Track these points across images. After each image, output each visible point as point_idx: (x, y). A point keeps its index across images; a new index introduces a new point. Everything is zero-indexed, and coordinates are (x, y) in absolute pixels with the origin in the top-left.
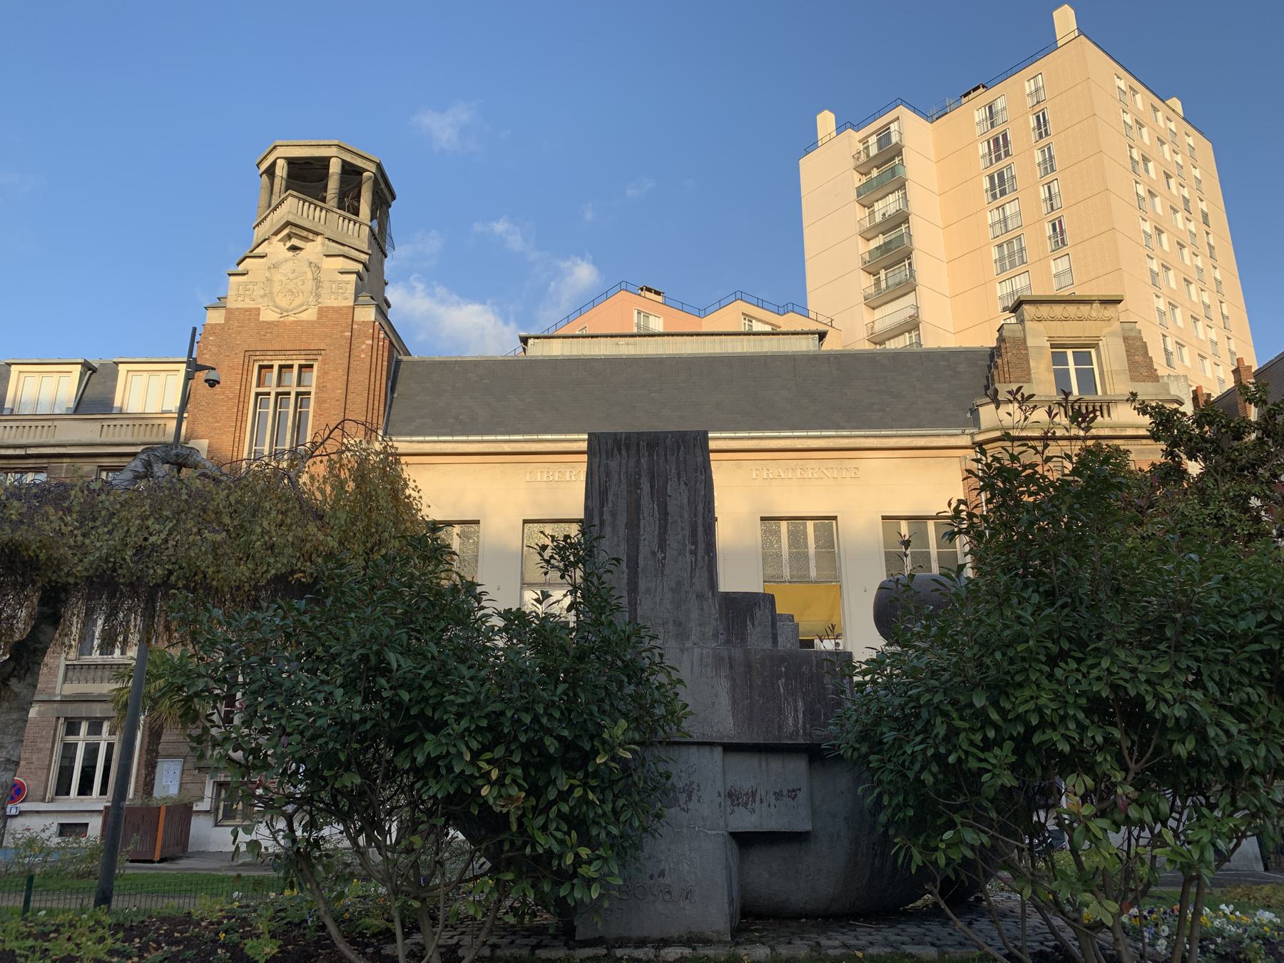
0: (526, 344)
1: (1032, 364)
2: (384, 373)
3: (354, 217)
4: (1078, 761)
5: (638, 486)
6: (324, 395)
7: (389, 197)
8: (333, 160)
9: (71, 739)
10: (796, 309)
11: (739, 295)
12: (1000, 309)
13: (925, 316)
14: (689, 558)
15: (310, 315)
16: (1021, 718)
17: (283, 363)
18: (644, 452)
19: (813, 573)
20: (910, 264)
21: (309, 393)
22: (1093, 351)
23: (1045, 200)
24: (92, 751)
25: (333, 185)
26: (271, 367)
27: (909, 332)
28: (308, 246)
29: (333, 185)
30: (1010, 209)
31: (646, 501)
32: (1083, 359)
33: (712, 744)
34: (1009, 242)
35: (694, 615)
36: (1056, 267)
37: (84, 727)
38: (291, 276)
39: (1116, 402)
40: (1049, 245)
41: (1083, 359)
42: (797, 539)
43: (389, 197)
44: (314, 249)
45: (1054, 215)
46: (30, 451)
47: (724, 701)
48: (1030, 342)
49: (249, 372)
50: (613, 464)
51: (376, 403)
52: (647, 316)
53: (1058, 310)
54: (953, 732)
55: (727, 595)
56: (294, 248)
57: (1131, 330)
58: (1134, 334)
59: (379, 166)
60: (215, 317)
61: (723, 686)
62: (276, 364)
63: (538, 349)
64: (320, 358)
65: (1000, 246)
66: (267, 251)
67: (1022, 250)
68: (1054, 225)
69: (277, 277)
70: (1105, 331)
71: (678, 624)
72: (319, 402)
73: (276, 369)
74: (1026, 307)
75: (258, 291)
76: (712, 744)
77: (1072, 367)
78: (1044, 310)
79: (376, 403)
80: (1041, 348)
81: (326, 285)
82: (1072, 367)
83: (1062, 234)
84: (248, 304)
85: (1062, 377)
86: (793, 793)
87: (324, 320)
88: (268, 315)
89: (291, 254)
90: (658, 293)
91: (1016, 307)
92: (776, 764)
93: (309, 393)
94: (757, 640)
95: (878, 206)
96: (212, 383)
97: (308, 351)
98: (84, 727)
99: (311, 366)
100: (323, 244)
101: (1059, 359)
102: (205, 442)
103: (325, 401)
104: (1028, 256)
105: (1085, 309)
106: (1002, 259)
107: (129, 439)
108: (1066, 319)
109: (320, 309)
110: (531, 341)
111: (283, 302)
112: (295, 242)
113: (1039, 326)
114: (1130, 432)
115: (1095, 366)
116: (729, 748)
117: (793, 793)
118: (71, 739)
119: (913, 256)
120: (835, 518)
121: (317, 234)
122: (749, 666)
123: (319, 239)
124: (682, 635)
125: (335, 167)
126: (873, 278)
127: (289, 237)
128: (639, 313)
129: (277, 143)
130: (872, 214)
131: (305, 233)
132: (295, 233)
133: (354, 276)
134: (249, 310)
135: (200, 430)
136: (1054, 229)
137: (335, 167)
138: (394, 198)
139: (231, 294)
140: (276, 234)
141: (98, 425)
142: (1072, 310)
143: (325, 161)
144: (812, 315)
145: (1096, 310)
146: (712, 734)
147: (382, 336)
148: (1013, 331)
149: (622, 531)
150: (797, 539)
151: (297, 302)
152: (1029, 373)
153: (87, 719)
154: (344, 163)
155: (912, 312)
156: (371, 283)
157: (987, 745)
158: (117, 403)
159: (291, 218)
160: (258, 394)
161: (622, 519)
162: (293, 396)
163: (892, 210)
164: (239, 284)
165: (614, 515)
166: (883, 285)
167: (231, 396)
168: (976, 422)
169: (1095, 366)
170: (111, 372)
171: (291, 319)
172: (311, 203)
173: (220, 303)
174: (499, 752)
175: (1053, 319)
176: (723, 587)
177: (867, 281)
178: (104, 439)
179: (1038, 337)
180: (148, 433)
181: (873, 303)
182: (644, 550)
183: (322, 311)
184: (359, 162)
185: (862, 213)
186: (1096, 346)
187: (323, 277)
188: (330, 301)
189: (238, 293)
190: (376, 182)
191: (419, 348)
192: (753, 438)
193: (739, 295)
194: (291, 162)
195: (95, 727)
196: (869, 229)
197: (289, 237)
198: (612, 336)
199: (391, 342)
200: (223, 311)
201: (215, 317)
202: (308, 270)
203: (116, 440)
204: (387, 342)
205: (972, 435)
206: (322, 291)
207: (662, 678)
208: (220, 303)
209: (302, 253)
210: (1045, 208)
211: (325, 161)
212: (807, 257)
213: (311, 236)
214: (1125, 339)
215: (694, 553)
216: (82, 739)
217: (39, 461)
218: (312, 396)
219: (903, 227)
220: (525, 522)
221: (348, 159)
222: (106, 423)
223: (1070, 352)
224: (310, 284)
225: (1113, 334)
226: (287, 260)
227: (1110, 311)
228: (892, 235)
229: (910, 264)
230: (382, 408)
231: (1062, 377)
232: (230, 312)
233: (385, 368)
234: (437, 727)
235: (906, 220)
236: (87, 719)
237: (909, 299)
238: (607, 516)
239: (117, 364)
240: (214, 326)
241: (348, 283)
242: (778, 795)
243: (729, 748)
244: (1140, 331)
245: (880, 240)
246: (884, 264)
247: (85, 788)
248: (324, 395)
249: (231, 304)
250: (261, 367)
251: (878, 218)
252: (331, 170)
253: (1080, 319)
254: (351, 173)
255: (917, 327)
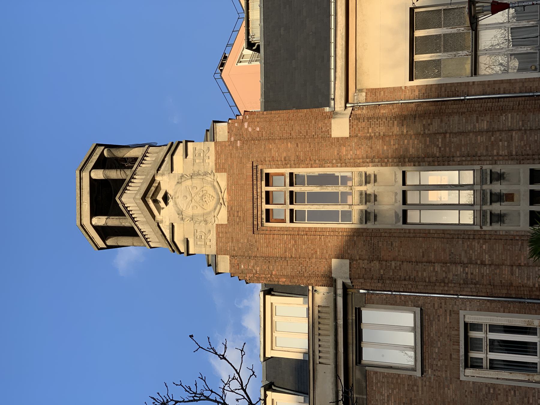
3: (139, 160)
6: (293, 158)
15: (222, 179)
17: (264, 200)
25: (114, 174)
26: (268, 211)
28: (164, 187)
29: (114, 174)
38: (189, 198)
42: (427, 45)
44: (166, 182)
46: (341, 322)
49: (272, 229)
56: (166, 198)
60: (224, 264)
63: (257, 35)
64: (260, 167)
69: (189, 212)
72: (299, 163)
75: (202, 228)
81: (196, 168)
84: (213, 236)
87: (226, 166)
88: (223, 217)
89: (171, 202)
93: (291, 174)
99: (267, 175)
100: (163, 175)
102: (334, 261)
103: (298, 157)
107: (331, 338)
109: (217, 170)
111: (212, 203)
112: (160, 197)
120: (412, 10)
121: (153, 180)
123: (158, 178)
125: (98, 175)
127: (156, 201)
129: (78, 223)
131: (153, 189)
134: (218, 234)
135: (322, 268)
139: (203, 251)
140: (154, 216)
141: (319, 367)
150: (427, 45)
151: (211, 191)
154: (95, 167)
158: (300, 357)
159: (139, 196)
164: (196, 244)
167: (293, 242)
170: (272, 363)
171: (226, 196)
173: (212, 263)
178: (331, 361)
180: (326, 321)
183: (219, 168)
187: (189, 172)
189: (204, 245)
194: (94, 213)
197: (156, 201)
200: (220, 257)
201: (224, 264)
203: (332, 350)
206: (202, 171)
208: (212, 263)
209: (171, 193)
211: (93, 182)
213: (155, 185)
217: (350, 341)
221: (93, 164)
222: (318, 360)
224: (196, 181)
232: (221, 251)
239: (266, 359)
240: (232, 265)
241: (195, 149)
248: (293, 158)
249: (212, 251)
250: (268, 220)
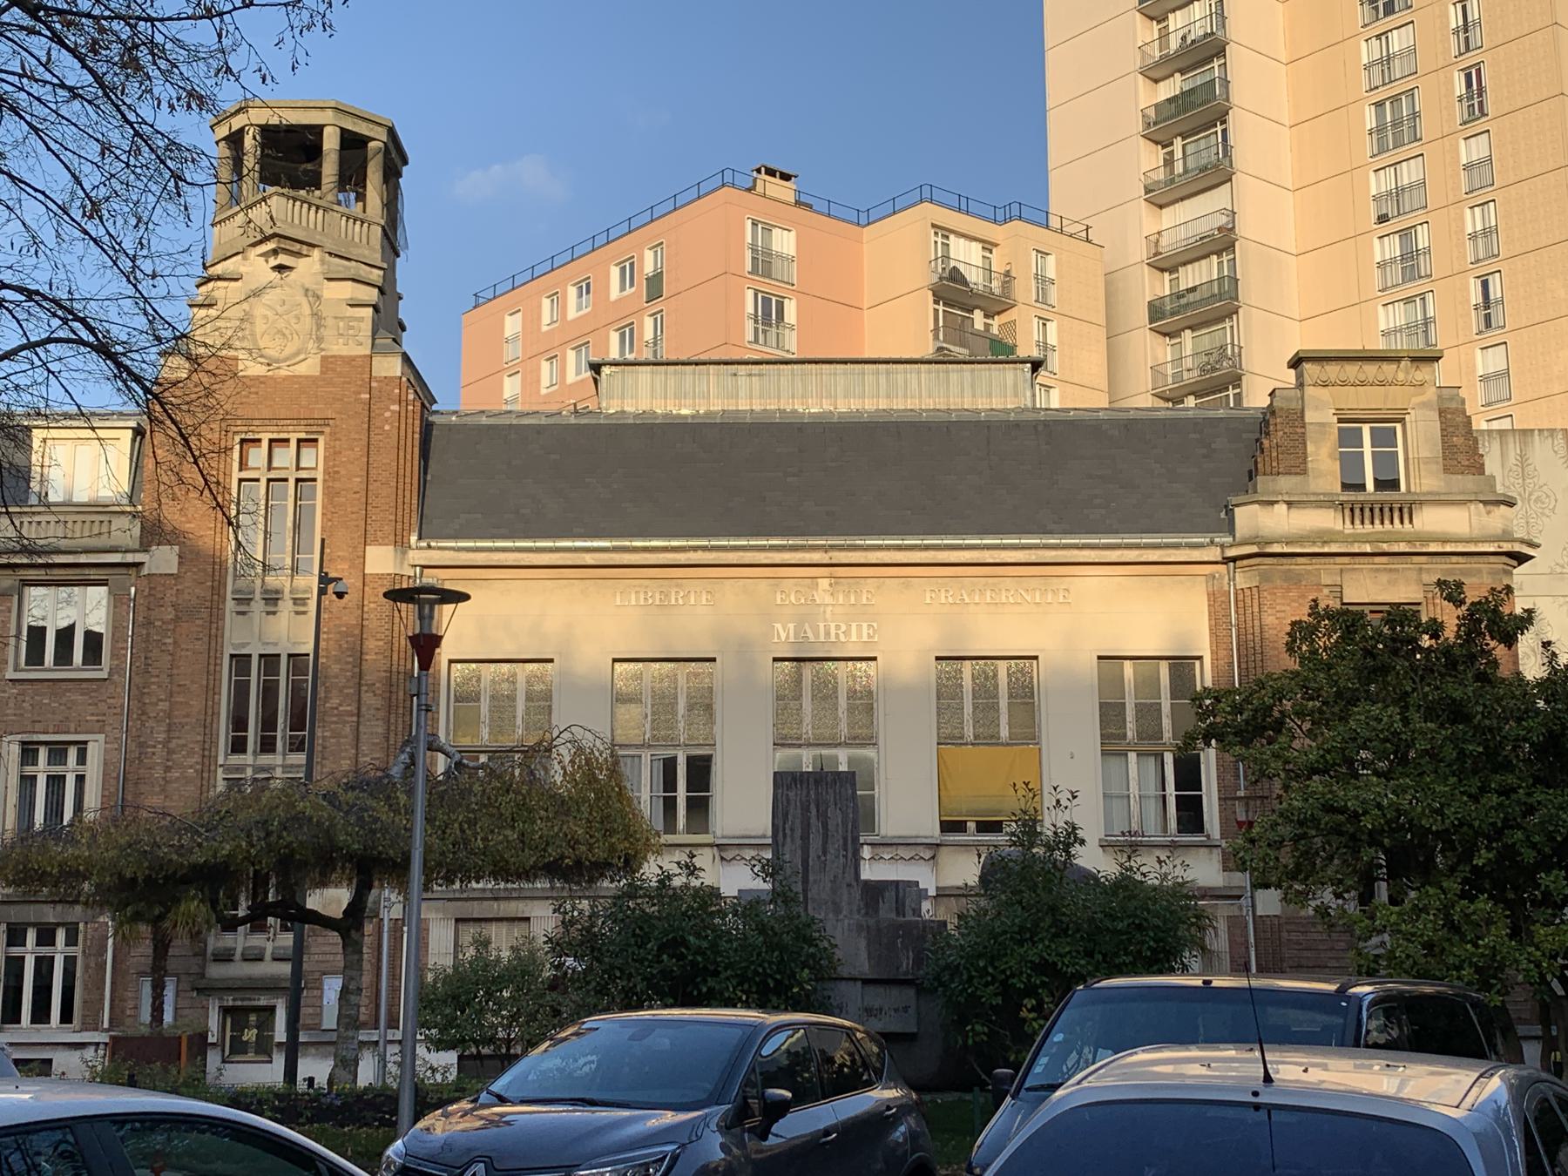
0: (598, 373)
1: (1310, 448)
2: (417, 450)
4: (1030, 991)
5: (808, 810)
6: (337, 485)
7: (398, 161)
8: (327, 130)
9: (16, 951)
10: (1026, 212)
11: (926, 192)
12: (1374, 218)
13: (1244, 229)
14: (842, 860)
15: (309, 367)
16: (1003, 972)
17: (275, 436)
18: (812, 786)
19: (1004, 733)
20: (1224, 131)
21: (314, 480)
22: (1398, 426)
23: (1456, 32)
24: (44, 965)
25: (330, 169)
27: (1219, 253)
29: (330, 169)
30: (1398, 41)
31: (813, 820)
32: (1384, 438)
33: (855, 980)
34: (1395, 99)
35: (845, 897)
36: (1469, 153)
37: (31, 936)
38: (280, 310)
39: (1421, 503)
40: (1459, 112)
41: (1384, 438)
43: (398, 161)
44: (308, 267)
45: (1470, 59)
46: (83, 559)
47: (864, 955)
48: (1310, 417)
50: (791, 794)
51: (408, 494)
52: (768, 229)
53: (1351, 370)
54: (971, 978)
55: (866, 882)
56: (280, 268)
57: (1451, 399)
58: (1454, 405)
59: (391, 132)
61: (863, 943)
62: (265, 437)
64: (327, 430)
65: (1379, 105)
66: (242, 269)
67: (1415, 115)
68: (1468, 77)
70: (1416, 400)
71: (834, 903)
72: (330, 493)
73: (265, 444)
74: (1307, 366)
76: (855, 980)
77: (1367, 449)
78: (1332, 370)
79: (408, 494)
80: (1323, 425)
81: (330, 322)
82: (1367, 449)
83: (1480, 95)
85: (1351, 464)
86: (906, 1009)
90: (786, 177)
91: (1296, 363)
92: (895, 991)
94: (886, 913)
95: (1176, 21)
96: (340, 595)
97: (309, 421)
98: (31, 936)
100: (322, 262)
101: (1349, 437)
104: (1425, 128)
105: (1389, 368)
106: (1380, 129)
108: (1363, 384)
110: (606, 370)
112: (283, 259)
113: (1324, 393)
114: (1433, 548)
115: (1400, 449)
116: (866, 982)
117: (906, 1009)
118: (16, 951)
119: (1231, 117)
120: (1036, 658)
121: (314, 246)
122: (879, 930)
123: (316, 253)
124: (837, 910)
125: (331, 141)
126: (1161, 152)
127: (275, 252)
128: (754, 224)
130: (1164, 36)
131: (297, 247)
132: (285, 246)
133: (371, 310)
136: (1469, 85)
137: (331, 141)
138: (405, 162)
140: (254, 245)
142: (1371, 370)
143: (318, 130)
144: (1054, 222)
145: (1402, 371)
146: (855, 973)
147: (411, 397)
148: (1288, 399)
149: (799, 842)
152: (1305, 462)
153: (33, 925)
155: (1223, 220)
156: (387, 322)
157: (987, 985)
160: (241, 480)
161: (798, 833)
162: (292, 483)
163: (1197, 32)
165: (792, 830)
166: (1179, 168)
168: (1231, 528)
169: (1400, 449)
171: (283, 373)
172: (295, 199)
174: (746, 986)
175: (1344, 384)
176: (864, 876)
177: (1150, 158)
179: (1321, 410)
181: (1161, 196)
182: (812, 854)
184: (362, 129)
185: (1147, 32)
186: (1401, 421)
187: (325, 310)
188: (338, 348)
190: (387, 151)
191: (457, 398)
192: (927, 548)
193: (926, 192)
194: (265, 130)
195: (46, 937)
196: (1157, 65)
197: (275, 252)
198: (726, 363)
199: (423, 405)
202: (304, 301)
204: (418, 404)
205: (1222, 546)
207: (826, 944)
209: (293, 275)
210: (1453, 44)
211: (318, 130)
212: (1050, 103)
214: (1442, 412)
215: (845, 856)
216: (30, 951)
218: (319, 485)
219: (1216, 63)
220: (615, 660)
223: (1366, 429)
224: (308, 323)
225: (1424, 405)
226: (270, 286)
227: (1423, 373)
228: (1197, 78)
229: (1224, 131)
230: (415, 501)
231: (1351, 464)
233: (417, 443)
234: (716, 973)
235: (1221, 52)
236: (33, 925)
237: (1216, 200)
238: (788, 831)
241: (361, 319)
242: (896, 1010)
243: (866, 982)
244: (1463, 402)
245: (1171, 87)
246: (1183, 128)
247: (41, 1014)
248: (337, 485)
251: (1174, 43)
252: (326, 147)
253: (1382, 384)
254: (353, 143)
255: (1230, 247)
